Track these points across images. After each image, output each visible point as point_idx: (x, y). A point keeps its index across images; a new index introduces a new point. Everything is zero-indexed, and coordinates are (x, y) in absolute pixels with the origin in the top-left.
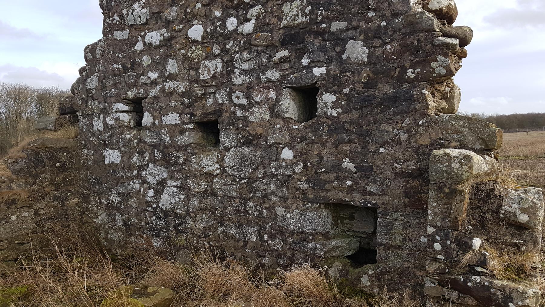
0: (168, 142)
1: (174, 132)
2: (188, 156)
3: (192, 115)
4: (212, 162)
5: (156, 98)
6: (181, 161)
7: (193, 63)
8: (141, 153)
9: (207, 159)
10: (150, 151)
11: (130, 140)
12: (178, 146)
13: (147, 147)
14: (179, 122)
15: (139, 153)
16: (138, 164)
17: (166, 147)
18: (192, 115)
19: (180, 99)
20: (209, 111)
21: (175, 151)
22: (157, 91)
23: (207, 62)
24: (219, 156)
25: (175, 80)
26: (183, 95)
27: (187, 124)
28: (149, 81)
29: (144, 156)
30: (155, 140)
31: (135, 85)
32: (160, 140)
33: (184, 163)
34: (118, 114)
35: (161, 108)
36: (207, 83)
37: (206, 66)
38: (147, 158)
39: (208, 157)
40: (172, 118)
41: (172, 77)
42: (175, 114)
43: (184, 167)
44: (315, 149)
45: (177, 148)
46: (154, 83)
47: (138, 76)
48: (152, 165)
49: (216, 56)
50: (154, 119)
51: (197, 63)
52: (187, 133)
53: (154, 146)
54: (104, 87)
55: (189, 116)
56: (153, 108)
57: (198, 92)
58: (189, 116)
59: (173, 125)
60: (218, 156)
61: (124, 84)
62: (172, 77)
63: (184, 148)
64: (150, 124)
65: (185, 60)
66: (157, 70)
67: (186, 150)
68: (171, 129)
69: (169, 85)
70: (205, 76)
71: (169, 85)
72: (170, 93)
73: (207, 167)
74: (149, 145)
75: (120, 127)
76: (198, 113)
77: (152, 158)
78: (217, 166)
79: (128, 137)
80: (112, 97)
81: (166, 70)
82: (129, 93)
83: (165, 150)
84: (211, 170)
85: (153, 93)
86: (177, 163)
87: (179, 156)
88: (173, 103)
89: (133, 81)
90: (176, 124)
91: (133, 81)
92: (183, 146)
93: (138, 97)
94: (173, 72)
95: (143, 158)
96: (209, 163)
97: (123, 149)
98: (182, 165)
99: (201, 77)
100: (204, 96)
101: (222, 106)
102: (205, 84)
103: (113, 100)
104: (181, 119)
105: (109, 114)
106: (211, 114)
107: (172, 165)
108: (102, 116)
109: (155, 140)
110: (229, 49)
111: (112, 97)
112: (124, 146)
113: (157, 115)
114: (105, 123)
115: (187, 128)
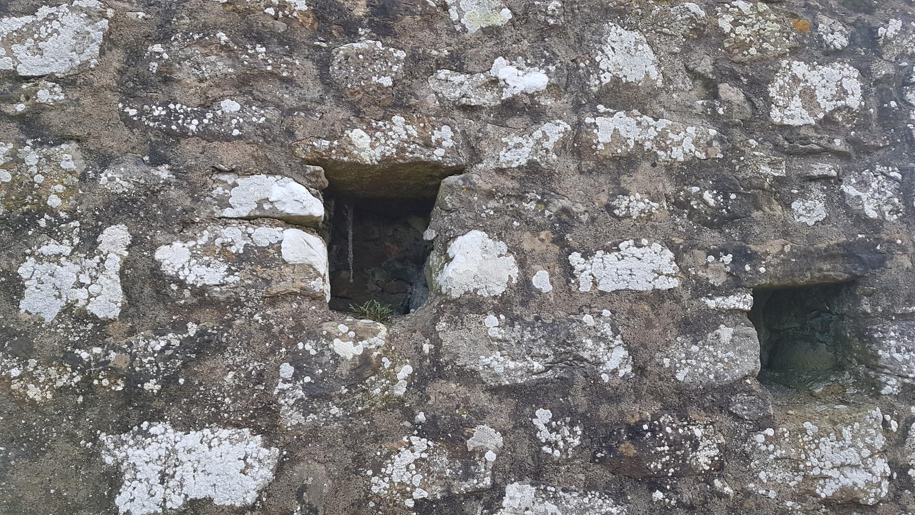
0: (614, 372)
1: (649, 324)
2: (732, 434)
3: (743, 256)
4: (866, 453)
5: (533, 172)
6: (704, 458)
7: (739, 57)
8: (449, 433)
9: (840, 437)
10: (503, 420)
11: (365, 363)
12: (680, 390)
13: (481, 398)
14: (674, 283)
15: (428, 430)
16: (419, 494)
17: (602, 394)
18: (743, 256)
19: (670, 189)
20: (822, 246)
21: (666, 408)
22: (549, 145)
23: (799, 68)
24: (894, 426)
25: (644, 112)
26: (689, 172)
27: (717, 291)
28: (488, 98)
29: (471, 444)
30: (537, 365)
31: (399, 101)
32: (569, 358)
33: (718, 467)
34: (264, 235)
35: (565, 220)
36: (806, 140)
37: (794, 78)
38: (491, 456)
39: (847, 432)
40: (643, 266)
41: (621, 96)
42: (657, 247)
43: (717, 483)
44: (708, 340)
45: (675, 400)
46: (521, 110)
47: (420, 65)
48: (529, 491)
49: (830, 55)
50: (521, 264)
51: (753, 61)
52: (726, 333)
53: (525, 396)
54: (139, 80)
55: (728, 258)
56: (518, 215)
57: (765, 169)
58: (728, 258)
59: (640, 296)
60: (885, 423)
61: (314, 90)
62: (621, 96)
63: (717, 398)
64: (499, 290)
65: (697, 41)
66: (540, 58)
67: (723, 407)
68: (632, 313)
69: (611, 128)
70: (793, 113)
71: (611, 128)
72: (616, 159)
73: (835, 473)
74: (494, 391)
75: (273, 300)
76: (774, 250)
77: (524, 451)
78: (881, 466)
79: (347, 350)
80: (228, 138)
81: (595, 65)
82: (359, 137)
83: (604, 411)
84: (861, 484)
85: (516, 149)
86: (686, 470)
87: (693, 439)
88: (635, 203)
89: (387, 81)
90: (657, 292)
91: (387, 81)
92: (709, 389)
93: (417, 163)
94: (633, 75)
95: (468, 460)
96: (852, 456)
97: (292, 418)
98: (708, 477)
99: (776, 115)
100: (782, 191)
101: (877, 231)
102: (791, 143)
103: (228, 154)
104: (684, 270)
105: (186, 224)
106: (829, 255)
107: (655, 482)
108: (115, 238)
109: (537, 365)
110: (887, 41)
111: (228, 138)
112: (317, 395)
113: (539, 247)
114: (146, 284)
115: (719, 311)
